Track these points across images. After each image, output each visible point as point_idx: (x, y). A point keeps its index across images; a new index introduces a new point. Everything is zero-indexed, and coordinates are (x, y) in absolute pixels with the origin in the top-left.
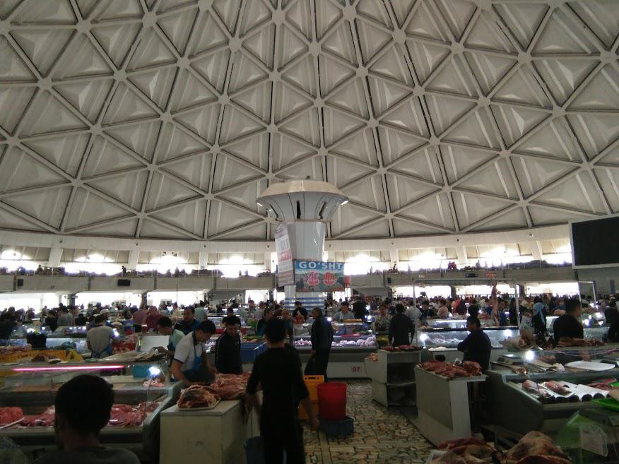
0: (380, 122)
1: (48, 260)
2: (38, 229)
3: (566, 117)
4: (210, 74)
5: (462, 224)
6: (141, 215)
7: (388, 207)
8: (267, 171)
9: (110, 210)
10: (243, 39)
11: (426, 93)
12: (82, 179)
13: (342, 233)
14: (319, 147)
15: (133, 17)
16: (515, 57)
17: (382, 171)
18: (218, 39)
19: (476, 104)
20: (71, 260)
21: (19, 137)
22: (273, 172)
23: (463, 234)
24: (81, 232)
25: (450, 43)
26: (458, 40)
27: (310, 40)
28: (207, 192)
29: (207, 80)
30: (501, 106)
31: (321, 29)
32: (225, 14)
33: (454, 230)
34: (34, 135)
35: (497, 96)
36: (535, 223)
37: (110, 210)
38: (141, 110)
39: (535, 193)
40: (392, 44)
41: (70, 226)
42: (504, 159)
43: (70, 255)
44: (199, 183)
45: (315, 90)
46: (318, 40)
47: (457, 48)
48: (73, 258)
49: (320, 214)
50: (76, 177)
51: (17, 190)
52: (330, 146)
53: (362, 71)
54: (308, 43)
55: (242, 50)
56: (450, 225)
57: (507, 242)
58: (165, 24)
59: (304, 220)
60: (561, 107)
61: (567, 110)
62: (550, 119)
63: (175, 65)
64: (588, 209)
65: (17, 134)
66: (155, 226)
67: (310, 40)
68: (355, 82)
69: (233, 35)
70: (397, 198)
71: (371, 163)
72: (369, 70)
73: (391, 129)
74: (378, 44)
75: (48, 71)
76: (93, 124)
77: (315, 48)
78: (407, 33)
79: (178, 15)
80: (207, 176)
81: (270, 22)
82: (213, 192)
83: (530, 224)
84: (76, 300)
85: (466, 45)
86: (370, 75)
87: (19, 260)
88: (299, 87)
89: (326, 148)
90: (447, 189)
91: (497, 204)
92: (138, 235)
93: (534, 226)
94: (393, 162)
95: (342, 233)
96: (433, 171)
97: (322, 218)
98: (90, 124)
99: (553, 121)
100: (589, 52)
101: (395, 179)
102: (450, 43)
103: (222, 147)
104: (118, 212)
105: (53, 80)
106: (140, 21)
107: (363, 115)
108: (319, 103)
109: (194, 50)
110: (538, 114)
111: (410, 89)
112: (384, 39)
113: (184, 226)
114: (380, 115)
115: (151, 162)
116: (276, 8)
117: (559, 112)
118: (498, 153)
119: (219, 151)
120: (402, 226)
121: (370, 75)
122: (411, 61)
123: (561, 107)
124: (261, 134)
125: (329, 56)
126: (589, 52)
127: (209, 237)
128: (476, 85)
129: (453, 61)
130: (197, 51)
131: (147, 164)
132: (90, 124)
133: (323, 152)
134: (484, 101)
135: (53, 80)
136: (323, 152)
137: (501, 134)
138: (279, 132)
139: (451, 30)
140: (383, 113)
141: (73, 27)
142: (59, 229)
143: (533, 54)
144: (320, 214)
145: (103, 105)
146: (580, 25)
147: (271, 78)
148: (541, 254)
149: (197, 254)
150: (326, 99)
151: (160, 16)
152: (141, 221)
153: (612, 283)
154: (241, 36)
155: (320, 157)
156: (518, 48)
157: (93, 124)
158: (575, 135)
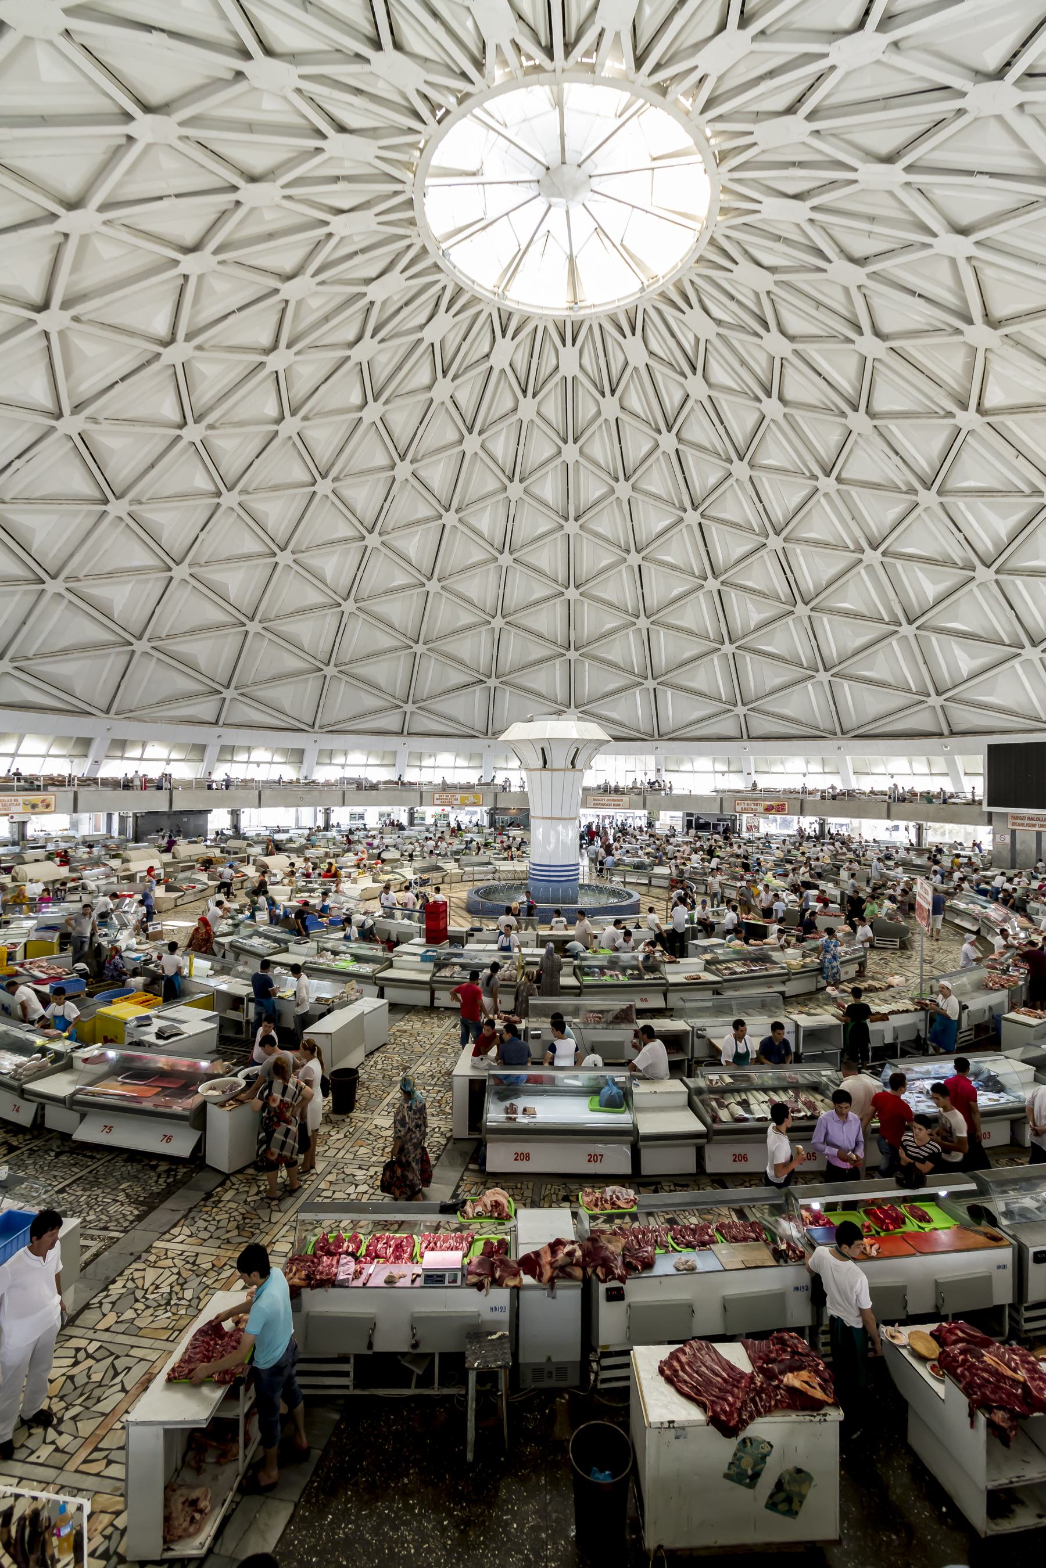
0: (722, 582)
1: (301, 763)
2: (289, 726)
3: (997, 582)
4: (485, 529)
5: (846, 726)
6: (409, 707)
7: (740, 697)
8: (568, 649)
9: (371, 702)
10: (525, 484)
11: (786, 545)
12: (336, 666)
13: (673, 731)
14: (638, 617)
15: (382, 469)
16: (914, 498)
17: (728, 648)
18: (492, 485)
19: (861, 560)
20: (229, 758)
21: (260, 622)
22: (425, 643)
23: (848, 739)
24: (334, 730)
25: (816, 478)
26: (828, 474)
27: (617, 480)
28: (490, 677)
29: (482, 537)
30: (899, 564)
31: (630, 464)
32: (499, 453)
33: (835, 734)
34: (278, 617)
35: (891, 549)
36: (955, 730)
37: (371, 702)
38: (401, 579)
39: (954, 687)
40: (731, 481)
41: (325, 722)
42: (906, 637)
43: (327, 756)
44: (479, 664)
45: (627, 543)
46: (627, 479)
47: (827, 484)
48: (331, 758)
49: (572, 763)
50: (328, 664)
51: (265, 682)
52: (653, 614)
53: (692, 517)
54: (613, 483)
55: (524, 497)
56: (828, 726)
57: (909, 754)
58: (422, 474)
59: (553, 770)
60: (989, 567)
61: (997, 572)
62: (972, 585)
63: (440, 522)
64: (1032, 713)
65: (258, 618)
66: (426, 721)
67: (617, 480)
68: (684, 530)
69: (511, 480)
70: (751, 684)
71: (712, 638)
72: (702, 515)
73: (739, 592)
74: (712, 481)
75: (287, 544)
76: (345, 600)
77: (623, 489)
78: (752, 466)
79: (440, 460)
80: (488, 659)
81: (560, 460)
82: (497, 677)
83: (946, 732)
84: (332, 815)
85: (839, 480)
86: (703, 521)
87: (269, 763)
88: (606, 539)
89: (648, 618)
90: (823, 676)
91: (899, 700)
92: (405, 732)
93: (952, 733)
94: (744, 637)
95: (673, 731)
96: (803, 651)
97: (574, 767)
98: (341, 601)
99: (978, 586)
100: (1027, 491)
101: (748, 660)
102: (816, 478)
103: (358, 605)
104: (379, 703)
105: (293, 553)
106: (391, 473)
107: (697, 574)
108: (634, 559)
109: (461, 502)
110: (951, 577)
111: (762, 540)
112: (719, 474)
113: (462, 720)
114: (721, 574)
115: (417, 642)
116: (565, 441)
117: (983, 574)
118: (896, 628)
119: (503, 625)
120: (761, 725)
121: (703, 521)
122: (761, 502)
123: (989, 567)
124: (558, 600)
125: (646, 499)
126: (1027, 490)
127: (320, 727)
128: (858, 533)
129: (823, 500)
130: (466, 502)
131: (412, 644)
132: (341, 601)
133: (643, 623)
134: (873, 557)
135: (293, 553)
136: (643, 623)
137: (900, 602)
138: (581, 598)
139: (817, 461)
140: (726, 571)
141: (312, 489)
142: (313, 726)
143: (940, 493)
144: (572, 763)
145: (382, 508)
146: (1009, 452)
147: (566, 530)
148: (851, 772)
149: (394, 753)
150: (643, 554)
151: (415, 465)
152: (408, 715)
153: (1039, 834)
154: (521, 481)
155: (640, 629)
156: (917, 486)
157: (345, 600)
158: (1012, 608)
